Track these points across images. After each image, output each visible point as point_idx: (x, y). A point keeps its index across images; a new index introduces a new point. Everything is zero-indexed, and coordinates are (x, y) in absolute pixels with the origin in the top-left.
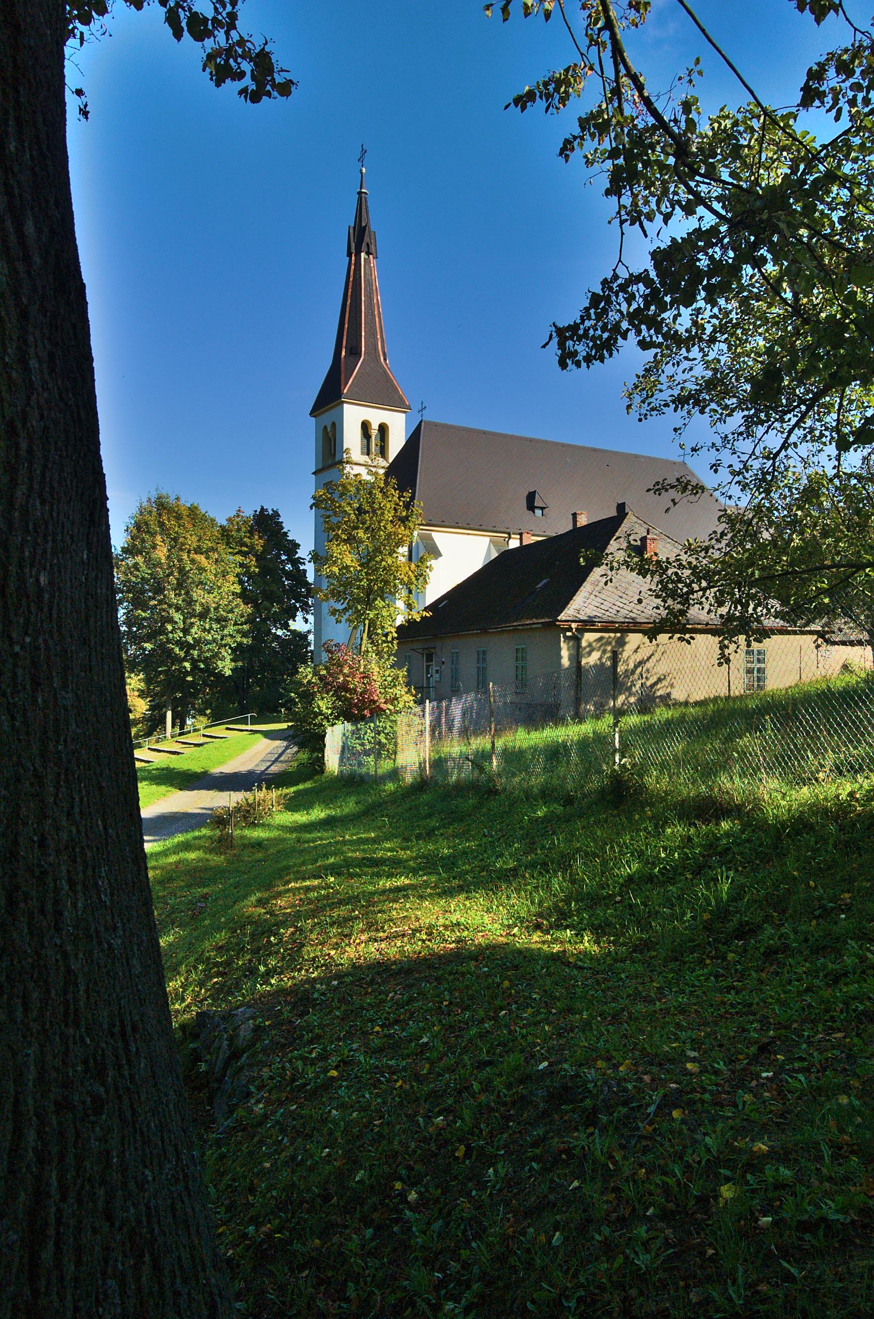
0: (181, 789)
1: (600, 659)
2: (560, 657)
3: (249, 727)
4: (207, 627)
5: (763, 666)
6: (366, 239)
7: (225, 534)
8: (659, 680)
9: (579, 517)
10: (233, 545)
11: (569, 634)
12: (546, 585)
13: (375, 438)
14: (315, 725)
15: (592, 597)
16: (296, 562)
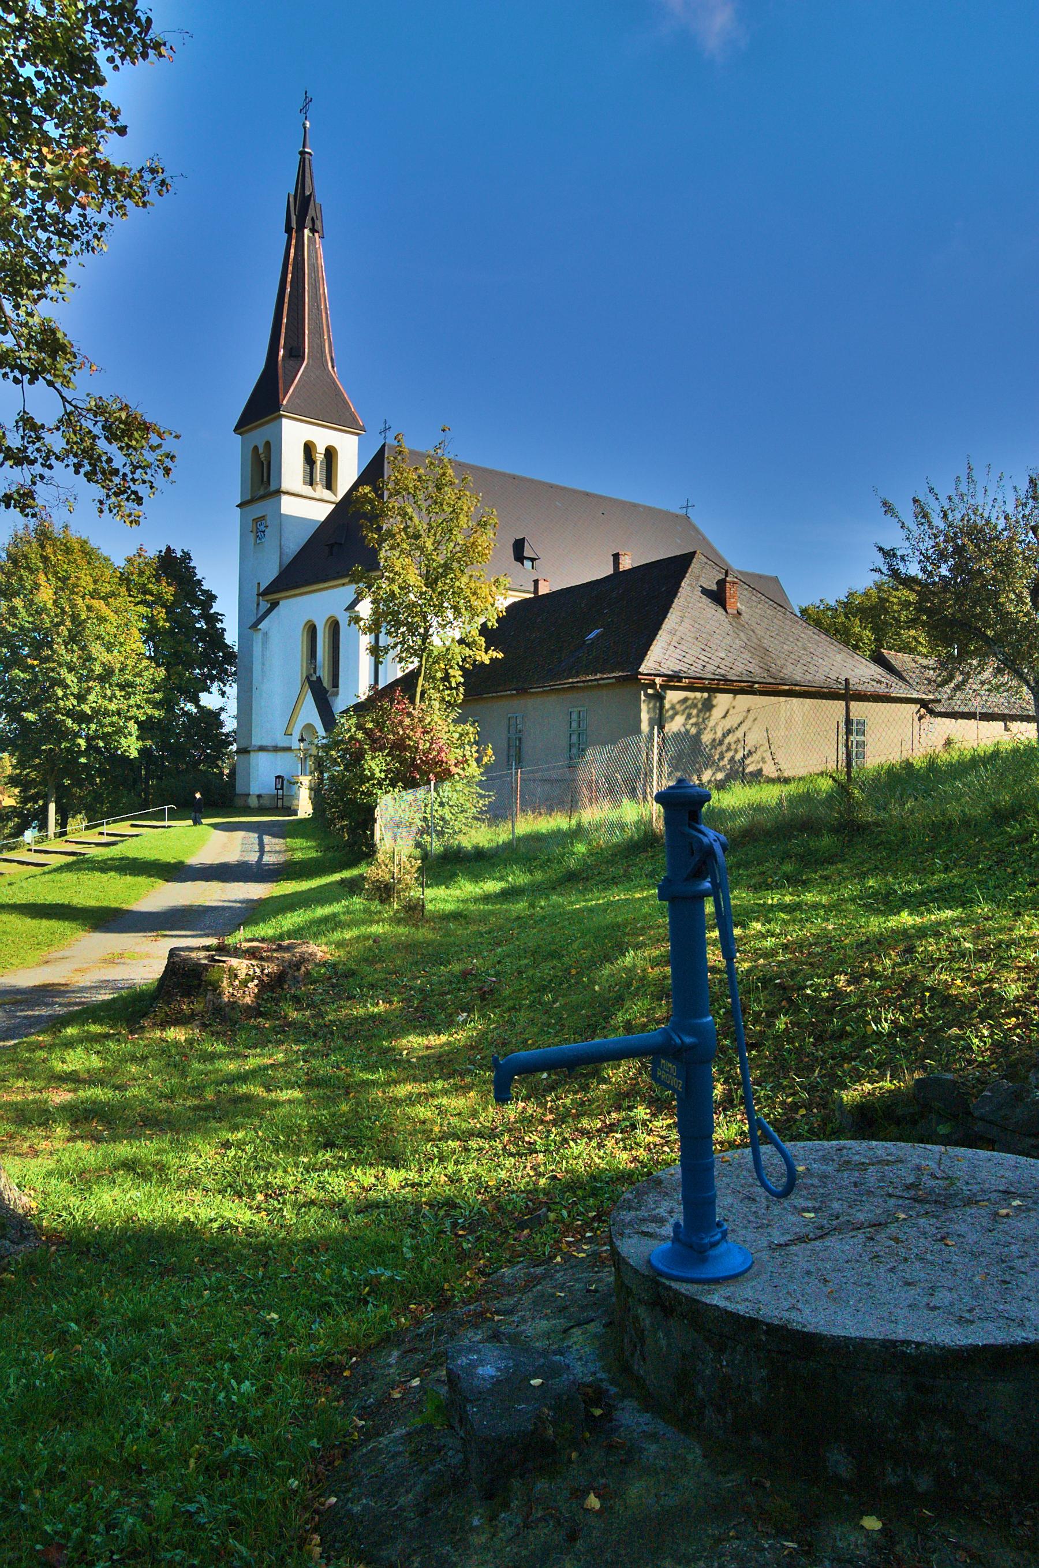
0: (167, 881)
1: (684, 725)
2: (640, 721)
3: (166, 823)
4: (109, 693)
5: (862, 738)
6: (311, 212)
7: (125, 579)
9: (622, 559)
10: (134, 593)
11: (650, 691)
12: (598, 637)
13: (321, 465)
14: (363, 793)
15: (672, 648)
16: (213, 619)
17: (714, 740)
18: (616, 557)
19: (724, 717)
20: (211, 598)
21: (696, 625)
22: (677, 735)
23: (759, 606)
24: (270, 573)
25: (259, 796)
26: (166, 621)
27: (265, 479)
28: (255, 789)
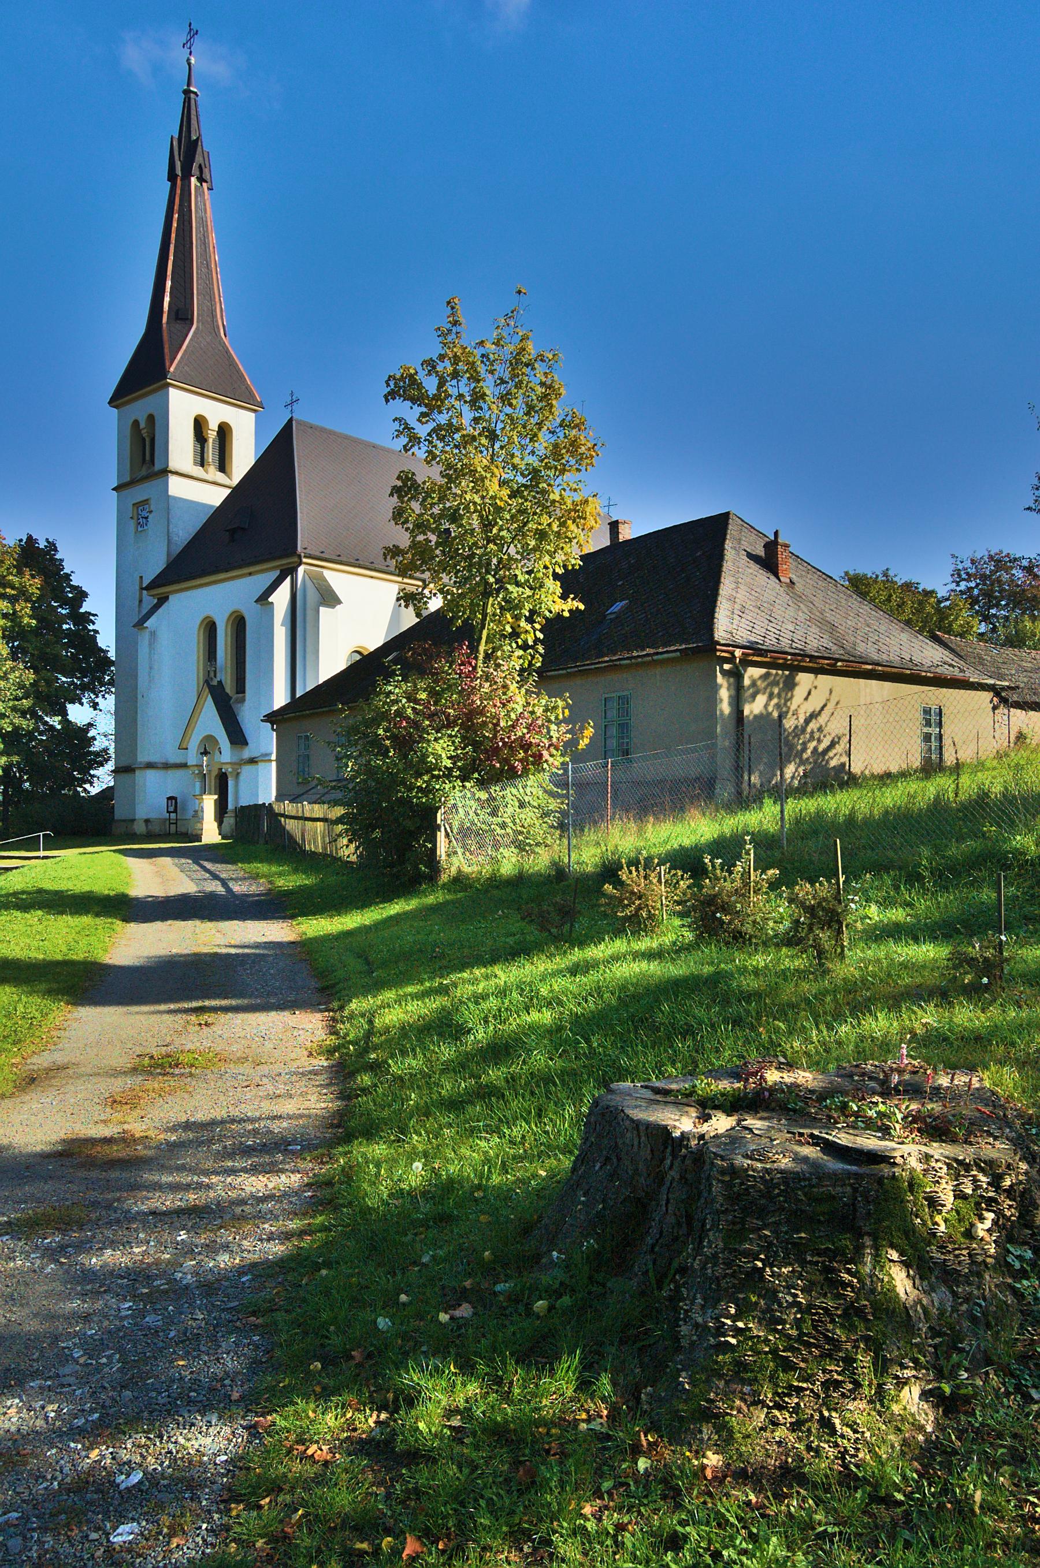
3: (42, 853)
5: (926, 730)
6: (199, 159)
8: (833, 745)
9: (621, 527)
11: (726, 667)
14: (420, 788)
16: (86, 618)
17: (796, 727)
18: (614, 526)
19: (806, 699)
20: (81, 595)
21: (753, 593)
22: (758, 718)
23: (809, 576)
24: (155, 564)
25: (147, 821)
26: (31, 617)
27: (148, 457)
28: (142, 813)
